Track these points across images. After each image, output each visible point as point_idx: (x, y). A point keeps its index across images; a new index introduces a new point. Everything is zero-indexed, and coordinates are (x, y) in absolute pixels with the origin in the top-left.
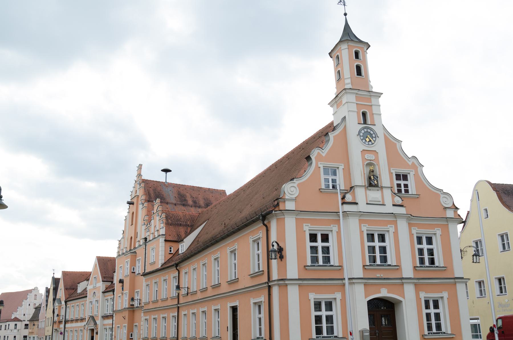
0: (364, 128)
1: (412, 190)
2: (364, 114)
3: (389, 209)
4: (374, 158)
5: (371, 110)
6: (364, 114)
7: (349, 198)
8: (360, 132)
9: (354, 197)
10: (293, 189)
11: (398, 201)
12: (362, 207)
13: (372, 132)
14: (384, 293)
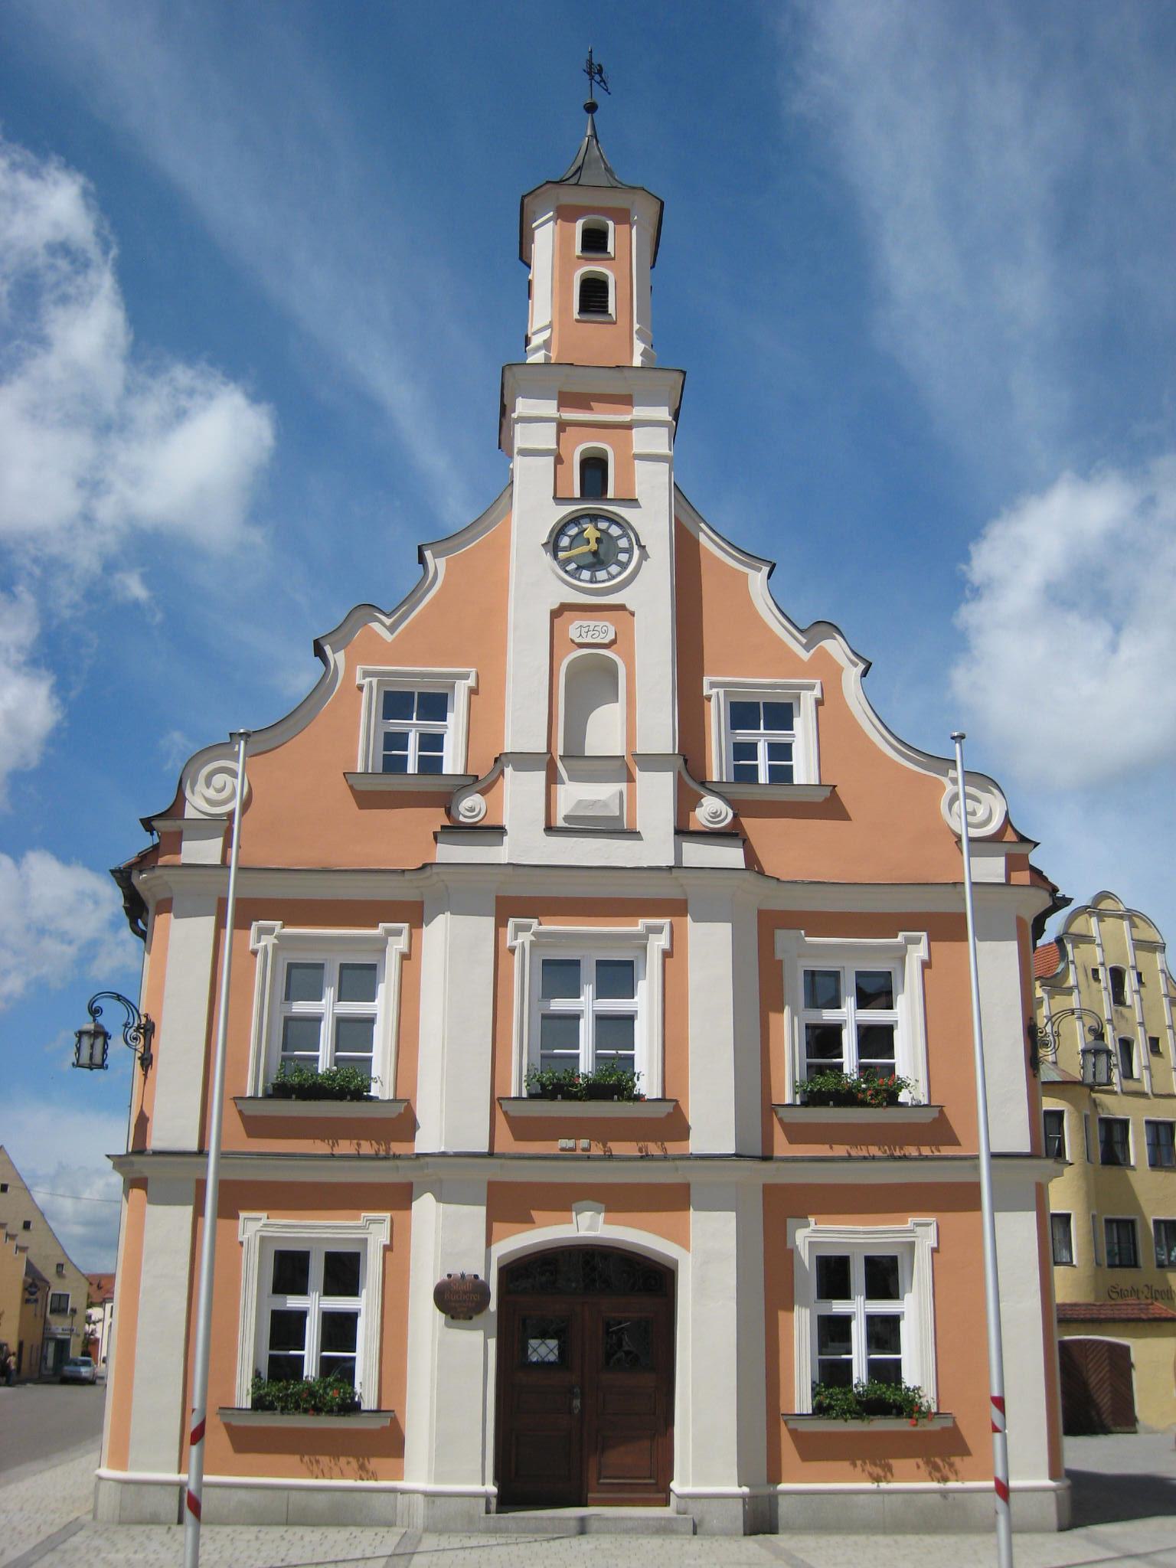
0: (575, 520)
1: (804, 770)
2: (594, 468)
3: (655, 846)
4: (611, 636)
5: (629, 443)
6: (594, 468)
7: (472, 807)
8: (559, 531)
9: (497, 806)
10: (219, 779)
11: (715, 815)
12: (525, 844)
13: (615, 531)
14: (588, 1226)
